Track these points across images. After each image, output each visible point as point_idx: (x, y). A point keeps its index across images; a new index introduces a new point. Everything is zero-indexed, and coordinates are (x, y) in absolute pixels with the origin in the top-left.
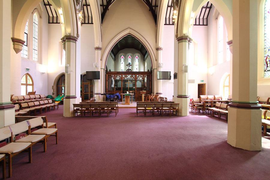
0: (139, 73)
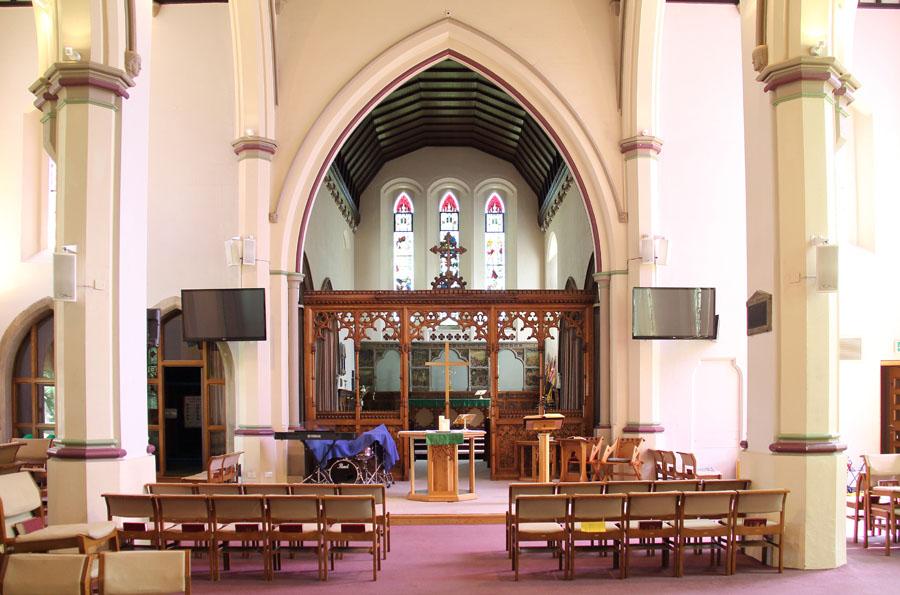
0: (514, 300)
